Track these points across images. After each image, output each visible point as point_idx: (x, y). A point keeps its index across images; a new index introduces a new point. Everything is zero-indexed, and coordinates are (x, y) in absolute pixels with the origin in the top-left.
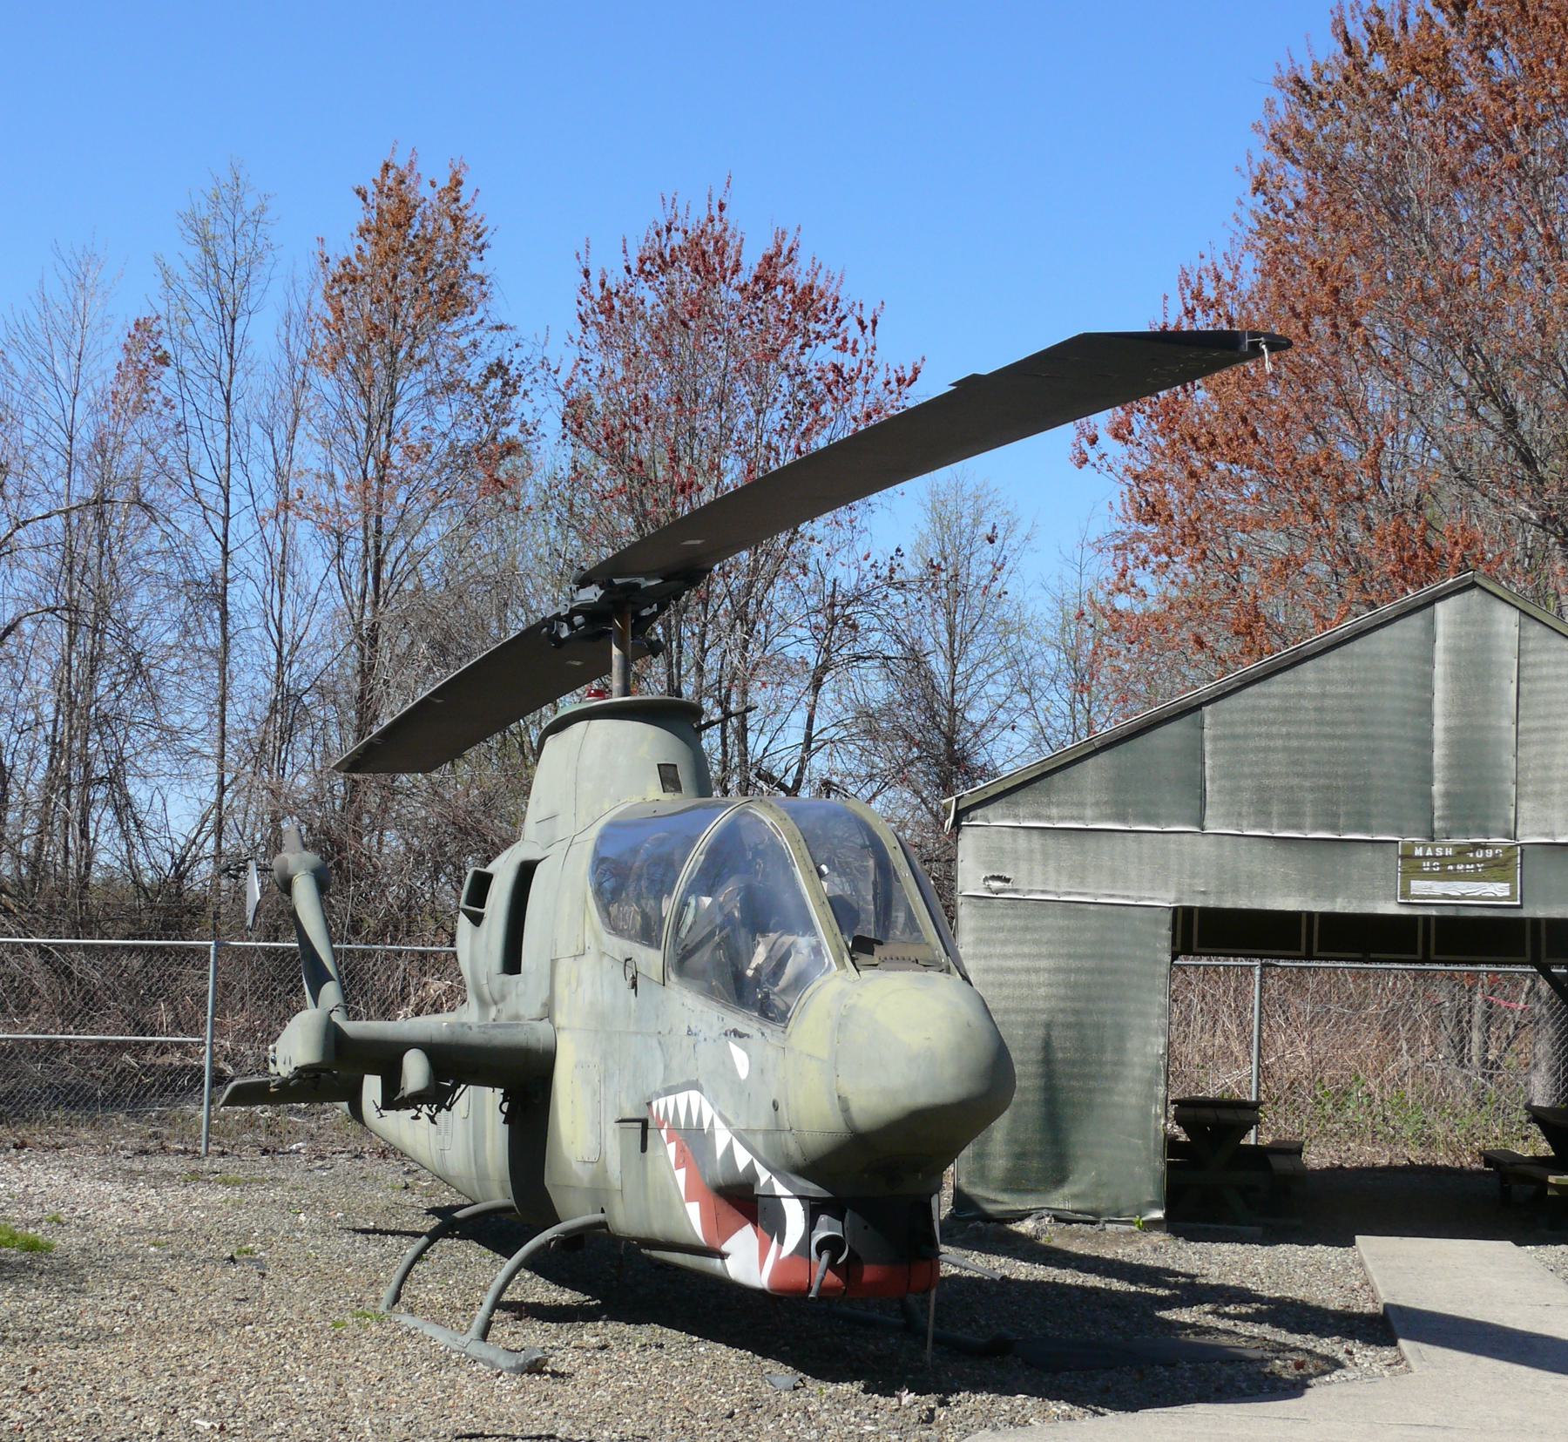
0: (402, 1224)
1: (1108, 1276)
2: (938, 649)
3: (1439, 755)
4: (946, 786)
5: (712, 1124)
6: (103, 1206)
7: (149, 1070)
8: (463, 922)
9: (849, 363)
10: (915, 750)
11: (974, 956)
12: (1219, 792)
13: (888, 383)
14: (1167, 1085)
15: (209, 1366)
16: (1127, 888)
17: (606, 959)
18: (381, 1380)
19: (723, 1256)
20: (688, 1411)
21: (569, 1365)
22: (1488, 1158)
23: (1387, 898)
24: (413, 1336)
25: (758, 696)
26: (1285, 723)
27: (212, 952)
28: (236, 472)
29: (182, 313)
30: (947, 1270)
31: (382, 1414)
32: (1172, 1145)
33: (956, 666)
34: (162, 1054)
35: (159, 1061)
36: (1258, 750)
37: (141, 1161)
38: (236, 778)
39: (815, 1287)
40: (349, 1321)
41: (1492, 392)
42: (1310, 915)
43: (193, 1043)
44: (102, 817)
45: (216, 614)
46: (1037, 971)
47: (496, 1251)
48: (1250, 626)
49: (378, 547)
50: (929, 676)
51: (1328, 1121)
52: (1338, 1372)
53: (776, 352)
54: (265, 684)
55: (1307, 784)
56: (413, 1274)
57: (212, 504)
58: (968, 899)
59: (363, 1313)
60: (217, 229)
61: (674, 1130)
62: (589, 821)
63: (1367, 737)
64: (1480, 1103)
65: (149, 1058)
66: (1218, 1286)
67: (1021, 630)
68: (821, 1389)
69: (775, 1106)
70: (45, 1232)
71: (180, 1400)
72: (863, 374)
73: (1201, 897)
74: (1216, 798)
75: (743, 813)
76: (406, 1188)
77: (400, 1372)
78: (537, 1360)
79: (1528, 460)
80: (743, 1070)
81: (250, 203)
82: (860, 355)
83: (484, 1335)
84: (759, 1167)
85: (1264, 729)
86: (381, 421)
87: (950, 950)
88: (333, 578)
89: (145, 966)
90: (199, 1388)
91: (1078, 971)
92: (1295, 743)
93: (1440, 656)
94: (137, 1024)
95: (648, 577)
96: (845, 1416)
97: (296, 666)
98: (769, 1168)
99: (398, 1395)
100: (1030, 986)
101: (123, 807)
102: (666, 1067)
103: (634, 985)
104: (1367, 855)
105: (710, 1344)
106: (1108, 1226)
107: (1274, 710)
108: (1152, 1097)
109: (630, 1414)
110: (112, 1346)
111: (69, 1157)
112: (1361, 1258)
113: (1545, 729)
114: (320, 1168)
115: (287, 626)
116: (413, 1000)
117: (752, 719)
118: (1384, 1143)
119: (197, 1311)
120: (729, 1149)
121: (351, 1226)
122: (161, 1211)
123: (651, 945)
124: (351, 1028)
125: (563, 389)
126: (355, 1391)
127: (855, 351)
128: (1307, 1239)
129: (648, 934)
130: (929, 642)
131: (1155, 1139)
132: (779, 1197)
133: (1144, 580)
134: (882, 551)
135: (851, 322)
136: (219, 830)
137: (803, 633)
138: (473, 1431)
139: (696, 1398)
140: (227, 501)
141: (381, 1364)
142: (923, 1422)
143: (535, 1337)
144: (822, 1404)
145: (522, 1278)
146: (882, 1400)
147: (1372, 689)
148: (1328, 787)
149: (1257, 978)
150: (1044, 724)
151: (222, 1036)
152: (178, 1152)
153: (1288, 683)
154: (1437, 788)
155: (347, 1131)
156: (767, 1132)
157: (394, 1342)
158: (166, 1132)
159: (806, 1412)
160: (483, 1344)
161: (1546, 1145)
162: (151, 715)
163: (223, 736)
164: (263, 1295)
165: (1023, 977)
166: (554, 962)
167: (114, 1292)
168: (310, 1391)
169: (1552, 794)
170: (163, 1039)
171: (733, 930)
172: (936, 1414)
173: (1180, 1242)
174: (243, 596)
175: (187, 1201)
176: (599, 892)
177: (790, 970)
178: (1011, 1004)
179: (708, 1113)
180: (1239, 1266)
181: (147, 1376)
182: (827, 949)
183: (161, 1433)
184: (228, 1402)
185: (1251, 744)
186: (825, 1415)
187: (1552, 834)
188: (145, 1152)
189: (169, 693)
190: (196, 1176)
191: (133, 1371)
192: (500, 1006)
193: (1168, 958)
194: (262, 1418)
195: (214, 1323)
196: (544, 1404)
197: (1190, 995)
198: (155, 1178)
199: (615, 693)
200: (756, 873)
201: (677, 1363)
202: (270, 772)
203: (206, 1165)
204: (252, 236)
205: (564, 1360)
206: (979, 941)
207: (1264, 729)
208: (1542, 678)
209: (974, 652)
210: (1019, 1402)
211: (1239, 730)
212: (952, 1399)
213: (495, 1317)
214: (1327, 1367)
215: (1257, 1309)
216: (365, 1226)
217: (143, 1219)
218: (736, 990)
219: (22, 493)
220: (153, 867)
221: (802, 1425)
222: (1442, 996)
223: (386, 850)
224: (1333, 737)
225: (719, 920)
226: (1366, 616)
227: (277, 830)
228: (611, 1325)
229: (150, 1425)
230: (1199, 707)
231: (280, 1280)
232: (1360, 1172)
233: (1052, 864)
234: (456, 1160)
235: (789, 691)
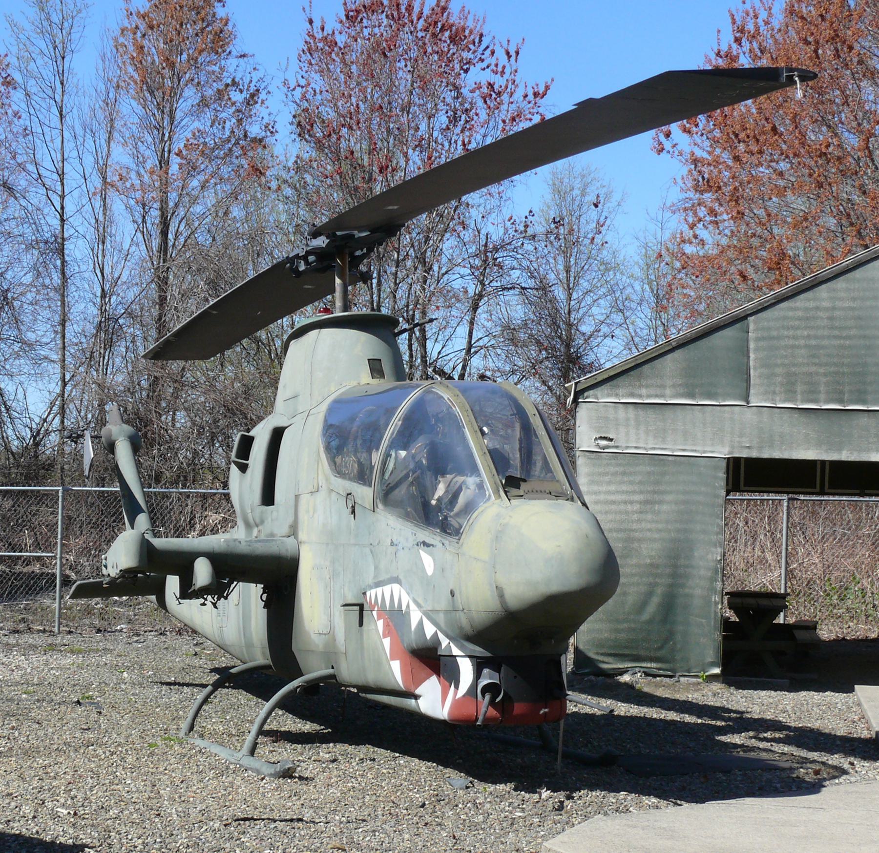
0: (193, 679)
1: (682, 713)
2: (559, 283)
4: (566, 377)
5: (408, 606)
7: (19, 575)
8: (234, 470)
9: (499, 82)
10: (544, 352)
11: (589, 493)
12: (760, 377)
13: (526, 96)
14: (723, 581)
15: (65, 773)
16: (694, 445)
17: (334, 494)
18: (182, 782)
19: (416, 697)
20: (393, 802)
21: (311, 772)
24: (203, 753)
26: (806, 328)
27: (60, 494)
30: (571, 708)
31: (184, 805)
32: (726, 624)
33: (571, 295)
34: (27, 565)
35: (25, 570)
36: (786, 347)
37: (15, 638)
38: (73, 376)
39: (481, 718)
40: (159, 743)
42: (823, 462)
43: (47, 557)
45: (59, 262)
46: (632, 502)
47: (258, 696)
48: (779, 264)
51: (834, 608)
52: (844, 777)
55: (821, 370)
56: (202, 712)
58: (583, 453)
59: (169, 738)
61: (382, 611)
62: (320, 399)
63: (865, 337)
65: (18, 568)
66: (759, 719)
67: (616, 268)
68: (485, 788)
69: (452, 594)
71: (46, 795)
72: (509, 90)
73: (747, 450)
74: (758, 381)
75: (428, 392)
76: (196, 654)
77: (195, 777)
78: (289, 769)
80: (430, 569)
82: (506, 76)
83: (252, 752)
84: (441, 636)
85: (791, 333)
87: (573, 485)
89: (13, 506)
90: (59, 787)
92: (813, 342)
94: (10, 544)
96: (502, 806)
97: (114, 298)
100: (627, 513)
102: (376, 568)
103: (353, 512)
104: (864, 420)
106: (682, 679)
107: (800, 319)
108: (713, 590)
109: (353, 805)
112: (859, 700)
114: (136, 642)
115: (107, 270)
116: (198, 526)
117: (431, 330)
118: (873, 623)
119: (55, 737)
120: (421, 624)
121: (159, 681)
122: (29, 670)
123: (364, 484)
124: (159, 543)
125: (298, 101)
126: (164, 789)
128: (820, 687)
129: (363, 476)
130: (552, 277)
131: (715, 618)
132: (455, 656)
134: (520, 214)
136: (63, 411)
138: (246, 816)
139: (398, 794)
140: (63, 184)
141: (182, 772)
142: (556, 810)
143: (287, 753)
144: (486, 799)
145: (277, 714)
146: (527, 796)
147: (868, 303)
148: (837, 373)
149: (785, 508)
150: (633, 334)
151: (67, 553)
152: (39, 631)
153: (809, 300)
155: (154, 617)
156: (446, 612)
157: (191, 757)
158: (31, 618)
159: (475, 804)
160: (252, 758)
162: (16, 332)
163: (64, 348)
164: (100, 726)
165: (622, 507)
166: (297, 497)
168: (134, 789)
170: (28, 554)
171: (422, 473)
172: (565, 804)
173: (732, 689)
175: (46, 665)
176: (328, 448)
177: (462, 500)
179: (406, 599)
180: (773, 706)
181: (24, 780)
182: (488, 485)
183: (34, 817)
184: (79, 797)
189: (26, 318)
190: (52, 647)
191: (14, 776)
192: (260, 528)
193: (724, 493)
194: (102, 807)
196: (294, 798)
197: (737, 521)
198: (24, 649)
199: (337, 310)
200: (438, 433)
201: (385, 771)
202: (97, 371)
203: (59, 640)
205: (308, 769)
206: (591, 482)
207: (791, 333)
209: (584, 284)
210: (622, 797)
212: (576, 795)
213: (259, 740)
214: (836, 774)
215: (786, 735)
216: (169, 681)
217: (17, 676)
218: (425, 515)
220: (18, 438)
221: (472, 812)
223: (178, 425)
225: (412, 466)
226: (861, 253)
227: (103, 411)
228: (339, 746)
229: (27, 811)
230: (745, 317)
231: (111, 716)
232: (857, 642)
233: (642, 428)
235: (454, 312)
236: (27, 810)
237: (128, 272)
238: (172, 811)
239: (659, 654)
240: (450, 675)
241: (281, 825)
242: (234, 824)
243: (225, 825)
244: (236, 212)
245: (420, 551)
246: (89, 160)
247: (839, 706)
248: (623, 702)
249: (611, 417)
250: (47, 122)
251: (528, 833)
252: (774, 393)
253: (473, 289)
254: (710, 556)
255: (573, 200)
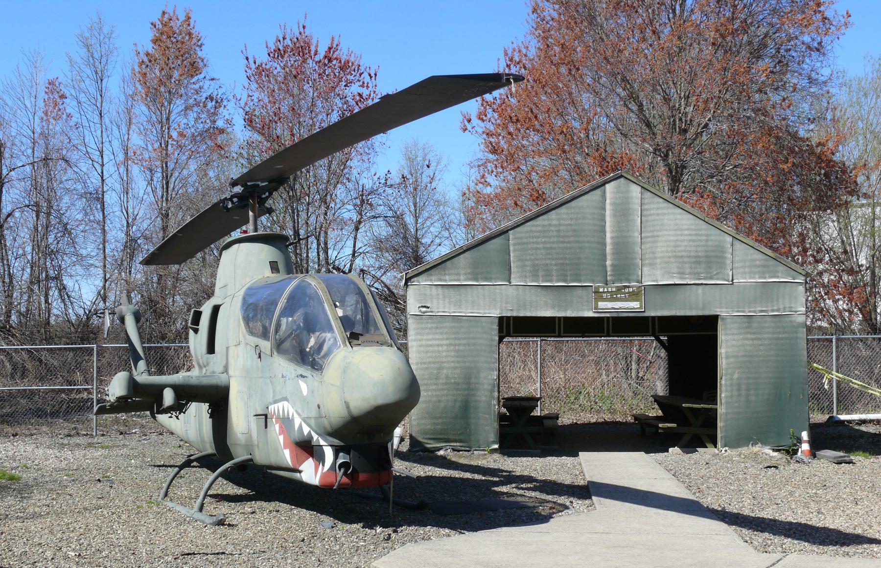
3: (609, 249)
5: (293, 415)
6: (47, 459)
8: (191, 332)
11: (416, 340)
16: (479, 309)
19: (300, 472)
22: (636, 418)
23: (588, 310)
25: (332, 234)
26: (543, 237)
28: (107, 145)
29: (78, 78)
32: (502, 417)
35: (77, 397)
36: (533, 249)
39: (337, 484)
41: (633, 96)
42: (559, 318)
44: (54, 293)
45: (99, 206)
46: (442, 345)
49: (167, 177)
50: (405, 226)
53: (334, 88)
54: (122, 236)
55: (554, 262)
57: (96, 160)
60: (93, 41)
63: (579, 242)
64: (635, 394)
65: (73, 396)
66: (519, 476)
67: (445, 204)
69: (319, 407)
70: (20, 472)
71: (64, 543)
72: (371, 97)
77: (163, 527)
79: (648, 125)
81: (106, 30)
82: (370, 89)
84: (313, 433)
85: (535, 240)
86: (165, 122)
88: (149, 189)
91: (459, 345)
92: (548, 246)
93: (608, 207)
95: (262, 182)
97: (134, 227)
98: (317, 434)
99: (160, 537)
100: (439, 352)
101: (62, 289)
102: (274, 392)
103: (260, 357)
104: (580, 292)
105: (300, 509)
106: (475, 452)
108: (492, 397)
110: (39, 520)
111: (36, 439)
113: (652, 237)
114: (144, 440)
115: (130, 210)
120: (300, 426)
127: (368, 87)
128: (559, 454)
129: (265, 335)
131: (494, 415)
133: (490, 179)
134: (382, 173)
135: (366, 75)
137: (351, 207)
140: (102, 157)
143: (224, 508)
147: (580, 221)
148: (563, 264)
152: (85, 435)
153: (544, 220)
154: (608, 263)
156: (316, 418)
161: (660, 411)
165: (436, 348)
166: (227, 348)
167: (45, 497)
169: (656, 263)
174: (111, 198)
175: (84, 456)
177: (325, 348)
178: (431, 360)
179: (291, 411)
182: (339, 339)
183: (53, 559)
185: (530, 246)
186: (343, 539)
187: (657, 281)
188: (69, 436)
189: (80, 240)
190: (90, 445)
191: (46, 531)
195: (85, 509)
196: (223, 539)
202: (126, 273)
203: (95, 440)
204: (108, 43)
206: (417, 334)
207: (535, 240)
208: (651, 215)
211: (525, 241)
217: (63, 465)
219: (12, 156)
222: (619, 350)
224: (564, 242)
225: (295, 327)
230: (507, 231)
232: (584, 425)
233: (447, 300)
234: (192, 434)
235: (344, 232)
236: (49, 554)
237: (143, 212)
238: (143, 550)
239: (461, 437)
240: (319, 458)
241: (210, 557)
242: (181, 557)
243: (175, 559)
244: (211, 174)
245: (300, 381)
246: (116, 144)
247: (568, 465)
248: (439, 467)
249: (428, 293)
250: (92, 120)
251: (366, 555)
252: (526, 276)
253: (355, 217)
254: (490, 377)
255: (418, 164)
